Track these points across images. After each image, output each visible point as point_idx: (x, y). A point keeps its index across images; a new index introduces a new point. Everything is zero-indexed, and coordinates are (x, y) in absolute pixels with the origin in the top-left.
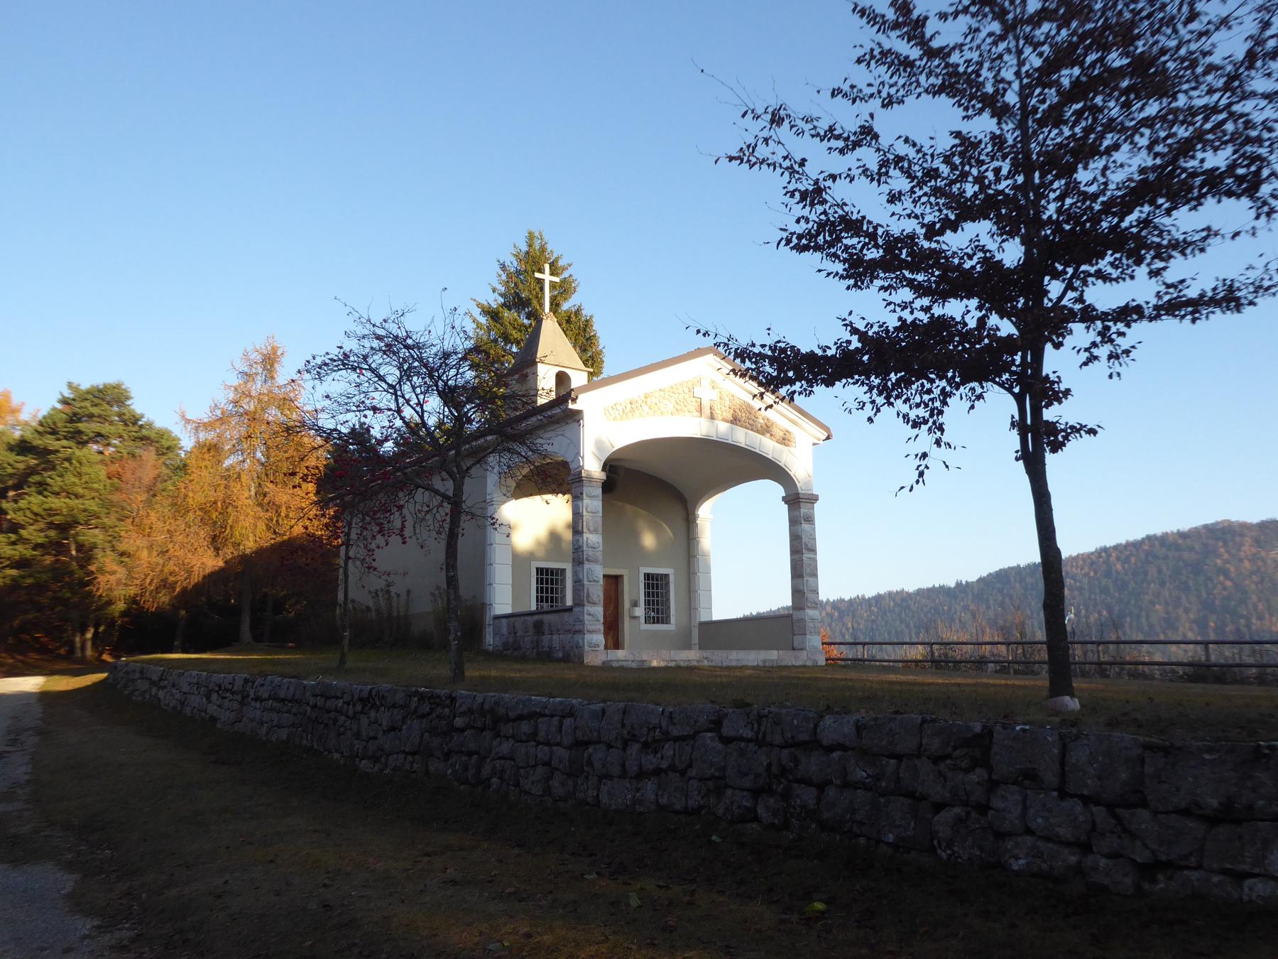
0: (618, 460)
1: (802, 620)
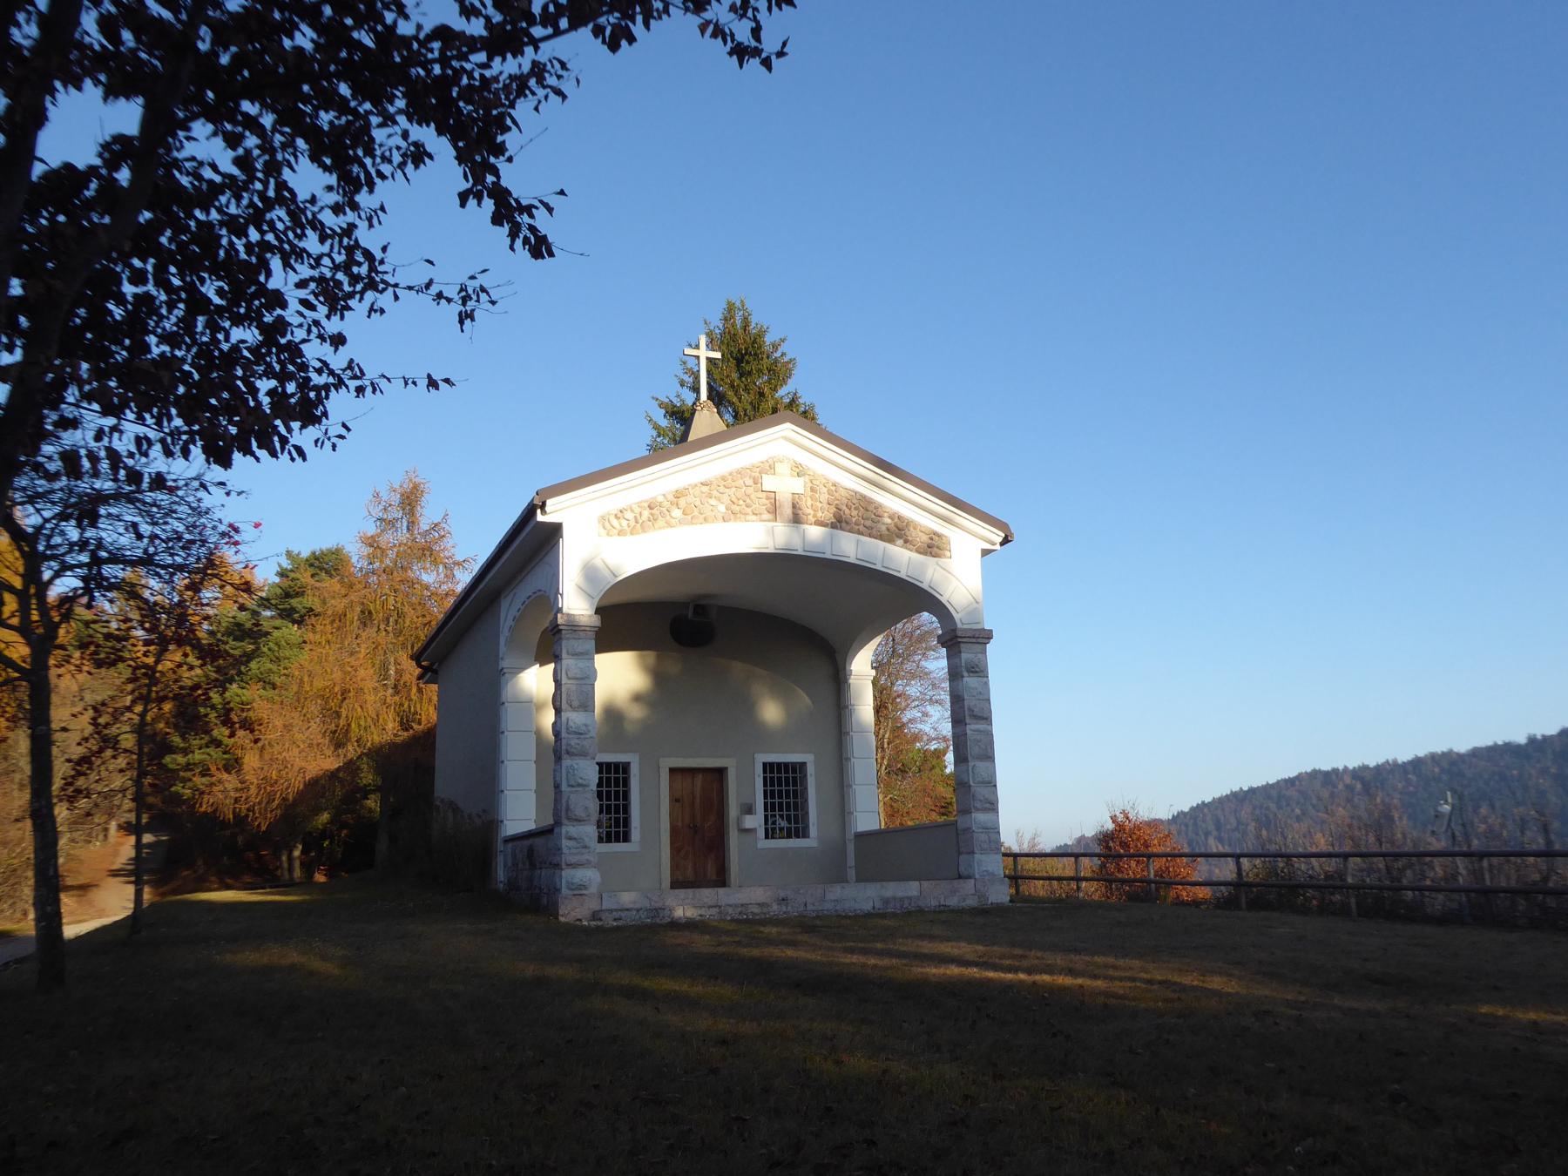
0: (706, 596)
1: (968, 830)
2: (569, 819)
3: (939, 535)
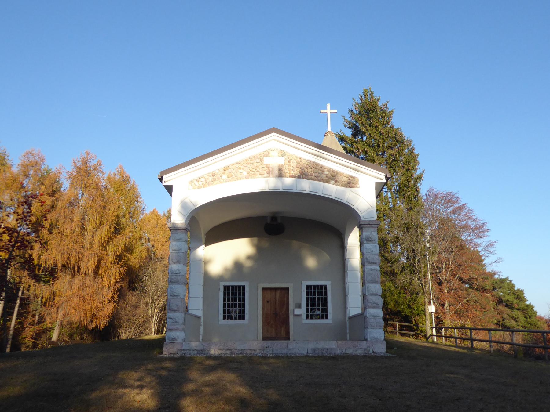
2: (170, 310)
3: (353, 178)
